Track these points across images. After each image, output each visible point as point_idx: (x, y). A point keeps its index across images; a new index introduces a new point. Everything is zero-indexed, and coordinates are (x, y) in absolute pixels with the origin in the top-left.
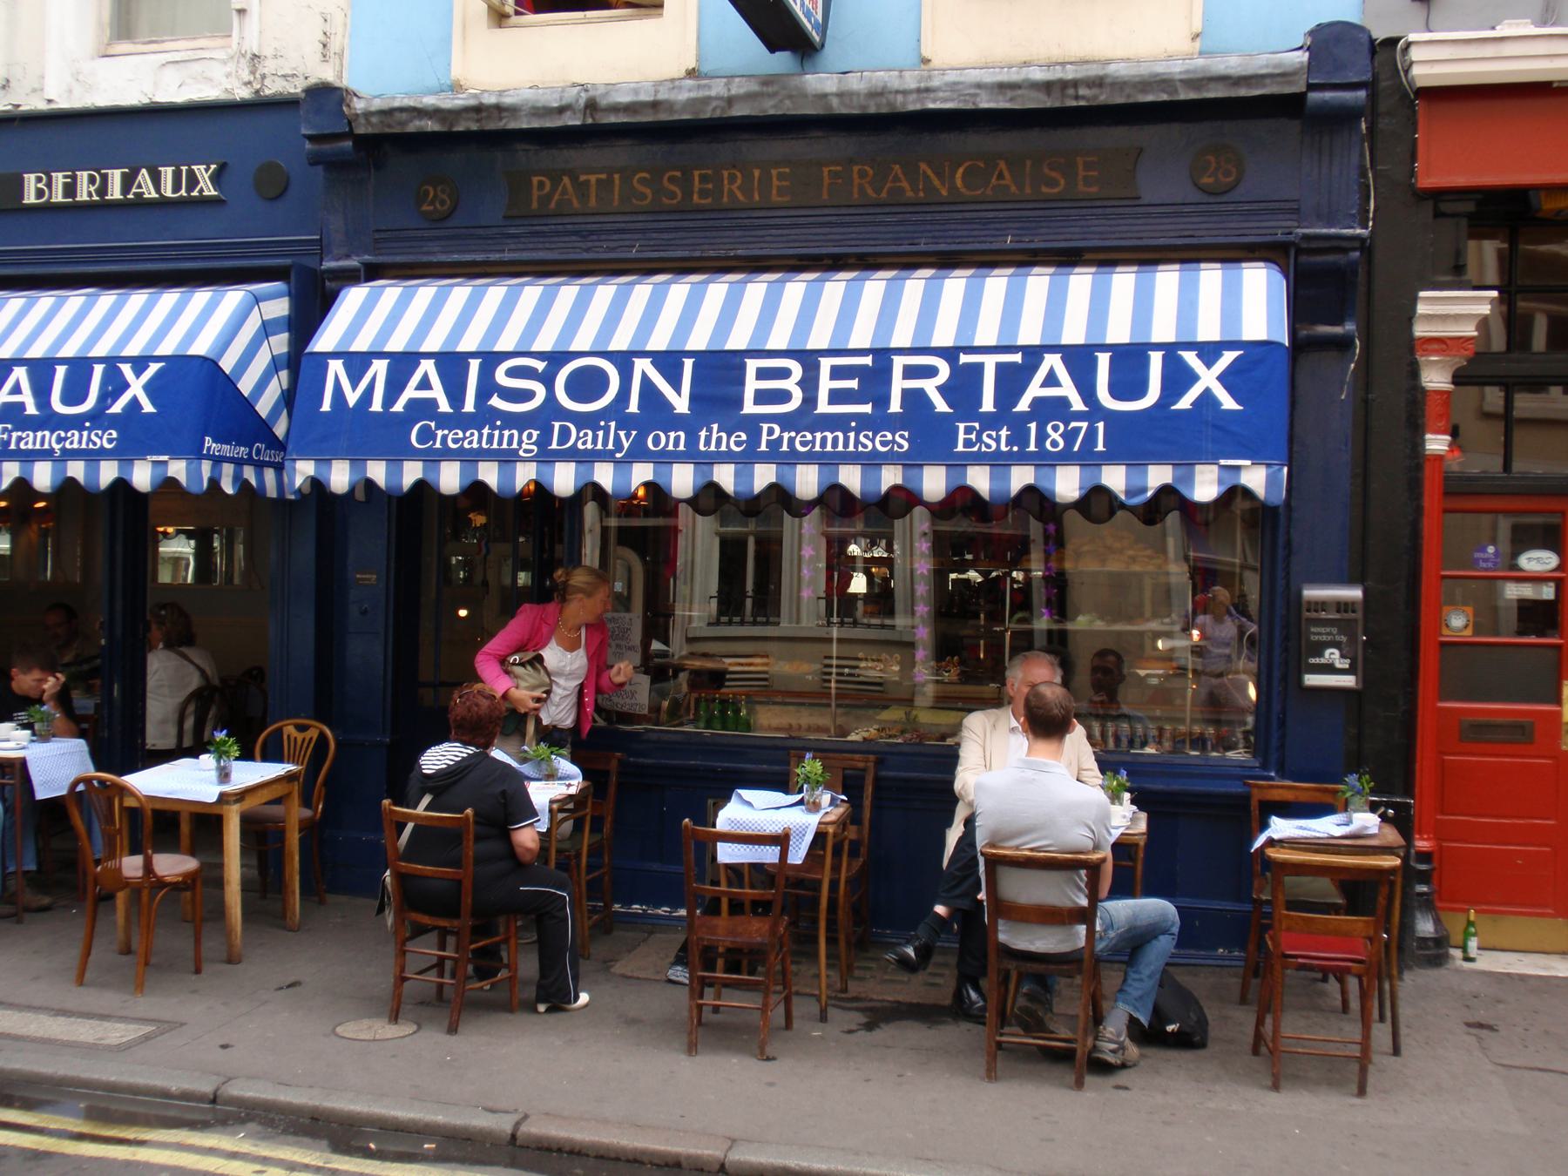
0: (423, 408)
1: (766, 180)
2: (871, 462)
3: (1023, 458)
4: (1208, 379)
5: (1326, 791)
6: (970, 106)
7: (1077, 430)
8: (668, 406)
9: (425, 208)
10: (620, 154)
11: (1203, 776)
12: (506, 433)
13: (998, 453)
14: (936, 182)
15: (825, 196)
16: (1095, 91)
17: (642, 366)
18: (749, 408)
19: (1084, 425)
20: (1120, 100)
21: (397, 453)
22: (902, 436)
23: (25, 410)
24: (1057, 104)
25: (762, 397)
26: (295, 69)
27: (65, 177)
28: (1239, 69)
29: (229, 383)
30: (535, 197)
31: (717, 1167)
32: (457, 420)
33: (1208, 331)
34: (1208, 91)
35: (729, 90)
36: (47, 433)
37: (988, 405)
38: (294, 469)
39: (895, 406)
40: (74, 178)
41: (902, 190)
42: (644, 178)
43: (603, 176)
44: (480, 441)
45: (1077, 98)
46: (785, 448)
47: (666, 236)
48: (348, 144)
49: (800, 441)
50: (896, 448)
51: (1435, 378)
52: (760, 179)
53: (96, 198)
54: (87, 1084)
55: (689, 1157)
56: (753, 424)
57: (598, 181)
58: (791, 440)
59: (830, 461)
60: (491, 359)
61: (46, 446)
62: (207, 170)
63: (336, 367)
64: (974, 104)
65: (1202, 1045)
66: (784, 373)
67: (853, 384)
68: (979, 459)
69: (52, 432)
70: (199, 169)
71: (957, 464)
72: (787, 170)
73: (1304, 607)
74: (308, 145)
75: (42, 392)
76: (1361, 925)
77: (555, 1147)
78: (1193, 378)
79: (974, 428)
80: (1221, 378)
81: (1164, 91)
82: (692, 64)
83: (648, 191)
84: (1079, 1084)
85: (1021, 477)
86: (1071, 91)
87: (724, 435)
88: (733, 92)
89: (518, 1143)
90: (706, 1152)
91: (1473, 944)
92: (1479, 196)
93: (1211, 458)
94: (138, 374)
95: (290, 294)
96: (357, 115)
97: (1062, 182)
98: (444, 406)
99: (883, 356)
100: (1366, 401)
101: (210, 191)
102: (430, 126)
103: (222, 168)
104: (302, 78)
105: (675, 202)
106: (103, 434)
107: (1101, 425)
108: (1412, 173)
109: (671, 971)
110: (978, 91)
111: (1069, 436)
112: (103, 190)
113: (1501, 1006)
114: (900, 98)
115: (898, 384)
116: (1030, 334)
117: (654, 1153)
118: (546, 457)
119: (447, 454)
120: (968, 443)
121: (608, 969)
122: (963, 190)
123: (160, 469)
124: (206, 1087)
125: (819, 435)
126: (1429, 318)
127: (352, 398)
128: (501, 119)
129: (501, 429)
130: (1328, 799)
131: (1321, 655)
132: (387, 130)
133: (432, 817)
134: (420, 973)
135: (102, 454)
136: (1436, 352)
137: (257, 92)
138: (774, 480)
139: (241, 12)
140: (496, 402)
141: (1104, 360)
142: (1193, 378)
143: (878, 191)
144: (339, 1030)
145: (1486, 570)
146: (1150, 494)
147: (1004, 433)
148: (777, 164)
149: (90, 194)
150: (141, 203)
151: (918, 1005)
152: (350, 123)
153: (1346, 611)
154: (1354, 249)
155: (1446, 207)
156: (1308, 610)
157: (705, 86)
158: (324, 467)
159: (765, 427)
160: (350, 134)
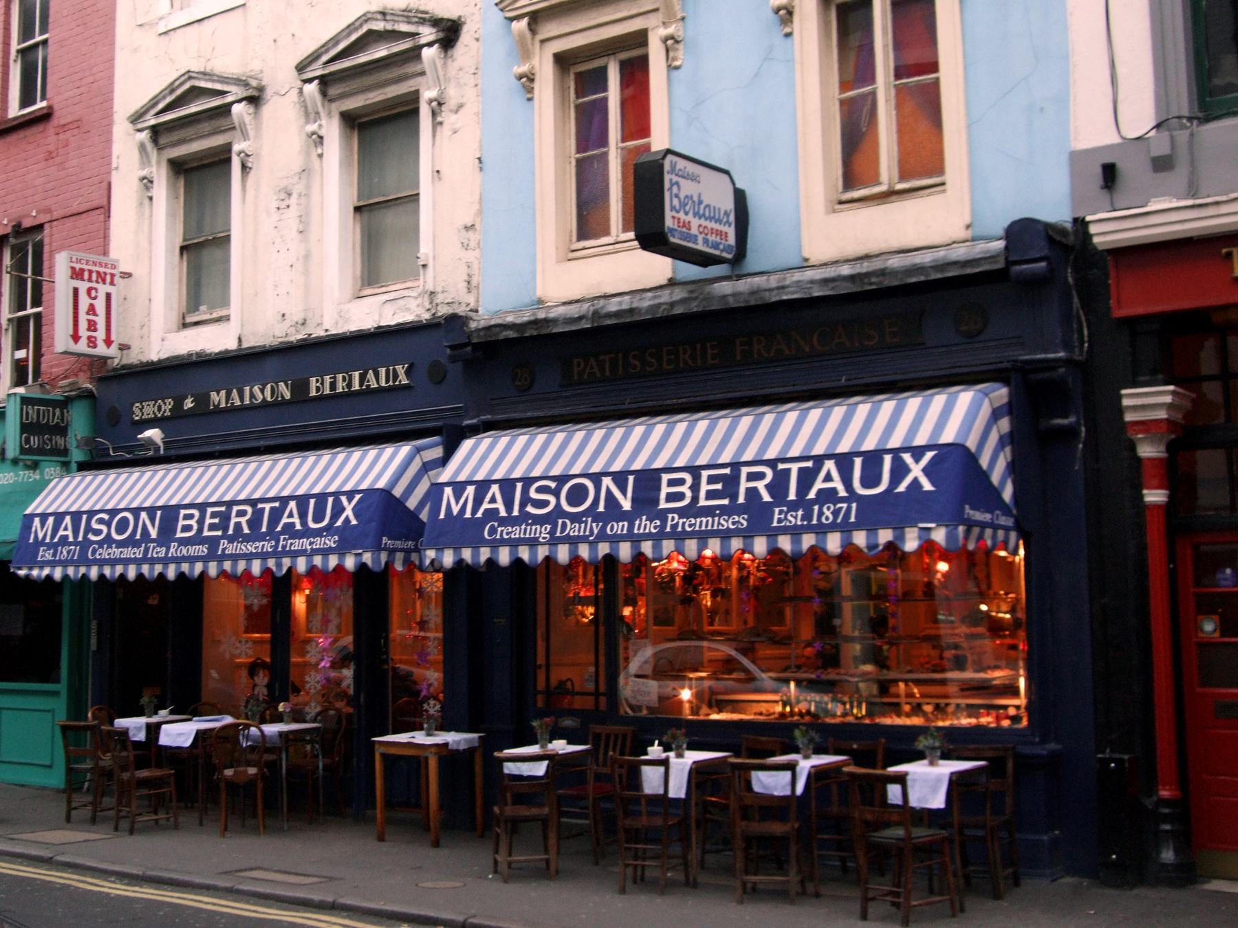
0: (492, 514)
3: (809, 529)
4: (916, 470)
6: (808, 296)
8: (619, 506)
9: (963, 328)
16: (881, 278)
17: (607, 482)
18: (663, 505)
19: (845, 505)
20: (895, 283)
22: (743, 518)
23: (295, 527)
24: (859, 289)
25: (671, 497)
26: (453, 298)
27: (331, 378)
29: (399, 503)
30: (576, 374)
32: (509, 521)
36: (538, 527)
37: (792, 496)
40: (335, 378)
43: (613, 355)
45: (871, 284)
46: (680, 529)
50: (740, 526)
58: (684, 524)
60: (528, 481)
63: (448, 491)
64: (810, 294)
66: (681, 482)
67: (719, 486)
68: (785, 530)
70: (399, 368)
71: (772, 534)
74: (448, 351)
75: (303, 515)
78: (344, 509)
81: (922, 275)
82: (669, 275)
83: (637, 363)
94: (917, 461)
96: (471, 331)
98: (503, 513)
99: (736, 466)
101: (405, 381)
102: (511, 334)
103: (411, 366)
104: (457, 303)
105: (653, 369)
106: (729, 518)
107: (854, 505)
111: (836, 513)
112: (350, 385)
115: (744, 485)
118: (554, 542)
120: (780, 521)
123: (359, 558)
127: (456, 510)
128: (549, 327)
129: (532, 525)
132: (489, 339)
134: (882, 896)
137: (434, 314)
139: (424, 266)
140: (530, 509)
145: (1228, 586)
146: (881, 548)
147: (800, 513)
149: (343, 389)
150: (369, 392)
159: (670, 516)
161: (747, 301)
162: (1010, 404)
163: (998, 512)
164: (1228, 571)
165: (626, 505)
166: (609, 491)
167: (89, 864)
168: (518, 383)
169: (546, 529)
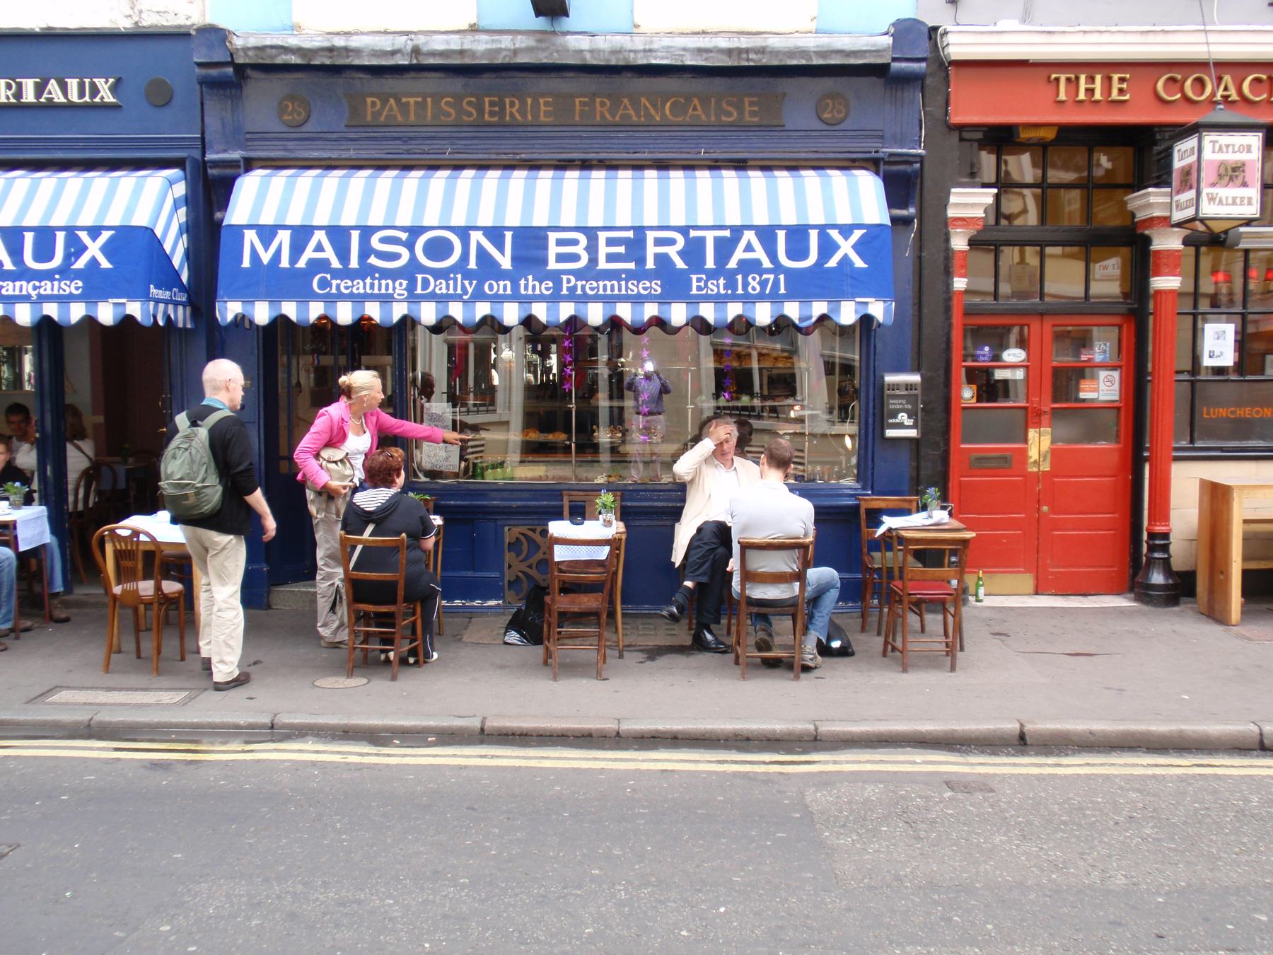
0: (319, 265)
1: (536, 105)
2: (638, 300)
3: (734, 298)
4: (846, 247)
5: (905, 500)
6: (679, 63)
7: (767, 280)
8: (495, 264)
9: (286, 117)
10: (431, 83)
11: (825, 496)
12: (383, 282)
13: (718, 296)
14: (652, 111)
15: (577, 118)
16: (760, 56)
17: (476, 237)
19: (771, 277)
20: (775, 63)
21: (304, 295)
22: (656, 284)
24: (736, 64)
25: (561, 258)
28: (850, 46)
31: (615, 734)
32: (346, 273)
33: (844, 218)
34: (831, 59)
35: (514, 44)
36: (24, 283)
37: (710, 263)
38: (226, 308)
39: (650, 264)
41: (629, 116)
42: (449, 102)
43: (420, 99)
44: (365, 288)
45: (748, 60)
46: (579, 292)
47: (463, 142)
48: (230, 70)
49: (590, 287)
50: (653, 292)
51: (959, 243)
52: (531, 105)
53: (12, 100)
54: (177, 725)
55: (597, 730)
56: (556, 276)
57: (416, 103)
59: (609, 300)
60: (367, 232)
61: (24, 292)
62: (106, 83)
63: (250, 236)
64: (682, 61)
65: (852, 654)
66: (575, 242)
67: (621, 249)
68: (707, 298)
69: (28, 282)
70: (100, 82)
72: (550, 100)
73: (886, 388)
74: (198, 70)
76: (953, 572)
77: (510, 733)
78: (836, 247)
79: (702, 279)
80: (854, 247)
81: (803, 58)
83: (452, 111)
84: (797, 678)
85: (734, 310)
86: (744, 56)
87: (537, 283)
88: (517, 46)
89: (486, 733)
90: (607, 726)
91: (981, 591)
92: (986, 129)
93: (851, 297)
95: (186, 179)
96: (237, 49)
97: (735, 114)
98: (336, 264)
100: (920, 258)
101: (110, 99)
103: (118, 81)
105: (472, 119)
107: (782, 277)
108: (947, 114)
109: (506, 638)
110: (683, 53)
111: (763, 284)
112: (19, 94)
113: (1006, 624)
114: (632, 55)
115: (651, 250)
116: (734, 219)
117: (574, 730)
119: (340, 297)
120: (699, 288)
121: (460, 640)
122: (670, 117)
123: (120, 309)
124: (266, 720)
125: (601, 284)
126: (956, 205)
127: (266, 257)
128: (348, 57)
129: (380, 279)
130: (906, 505)
131: (896, 417)
133: (377, 540)
135: (71, 298)
136: (960, 226)
137: (136, 23)
138: (573, 313)
140: (373, 260)
141: (781, 235)
142: (836, 247)
143: (613, 116)
144: (315, 683)
145: (984, 361)
146: (814, 319)
147: (722, 282)
148: (543, 95)
149: (8, 98)
150: (51, 106)
151: (670, 646)
152: (232, 55)
153: (911, 389)
154: (916, 162)
155: (966, 135)
156: (889, 390)
157: (497, 40)
158: (249, 306)
159: (565, 278)
160: (232, 63)
161: (608, 60)
162: (186, 196)
163: (175, 290)
164: (987, 349)
165: (505, 262)
166: (480, 247)
167: (217, 719)
168: (286, 117)
169: (401, 285)
